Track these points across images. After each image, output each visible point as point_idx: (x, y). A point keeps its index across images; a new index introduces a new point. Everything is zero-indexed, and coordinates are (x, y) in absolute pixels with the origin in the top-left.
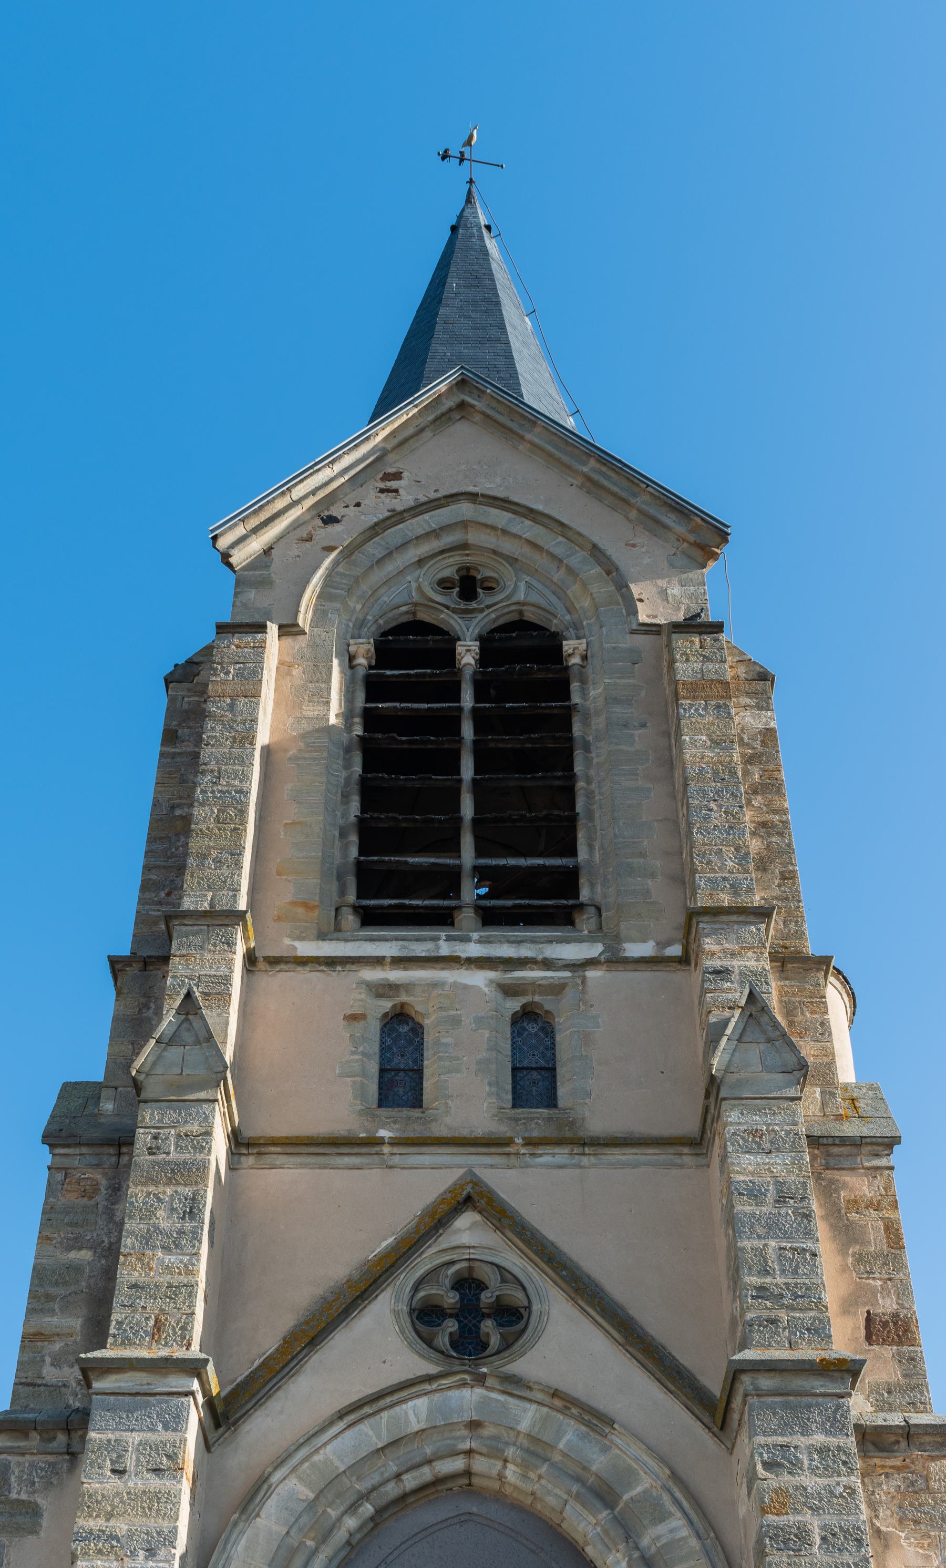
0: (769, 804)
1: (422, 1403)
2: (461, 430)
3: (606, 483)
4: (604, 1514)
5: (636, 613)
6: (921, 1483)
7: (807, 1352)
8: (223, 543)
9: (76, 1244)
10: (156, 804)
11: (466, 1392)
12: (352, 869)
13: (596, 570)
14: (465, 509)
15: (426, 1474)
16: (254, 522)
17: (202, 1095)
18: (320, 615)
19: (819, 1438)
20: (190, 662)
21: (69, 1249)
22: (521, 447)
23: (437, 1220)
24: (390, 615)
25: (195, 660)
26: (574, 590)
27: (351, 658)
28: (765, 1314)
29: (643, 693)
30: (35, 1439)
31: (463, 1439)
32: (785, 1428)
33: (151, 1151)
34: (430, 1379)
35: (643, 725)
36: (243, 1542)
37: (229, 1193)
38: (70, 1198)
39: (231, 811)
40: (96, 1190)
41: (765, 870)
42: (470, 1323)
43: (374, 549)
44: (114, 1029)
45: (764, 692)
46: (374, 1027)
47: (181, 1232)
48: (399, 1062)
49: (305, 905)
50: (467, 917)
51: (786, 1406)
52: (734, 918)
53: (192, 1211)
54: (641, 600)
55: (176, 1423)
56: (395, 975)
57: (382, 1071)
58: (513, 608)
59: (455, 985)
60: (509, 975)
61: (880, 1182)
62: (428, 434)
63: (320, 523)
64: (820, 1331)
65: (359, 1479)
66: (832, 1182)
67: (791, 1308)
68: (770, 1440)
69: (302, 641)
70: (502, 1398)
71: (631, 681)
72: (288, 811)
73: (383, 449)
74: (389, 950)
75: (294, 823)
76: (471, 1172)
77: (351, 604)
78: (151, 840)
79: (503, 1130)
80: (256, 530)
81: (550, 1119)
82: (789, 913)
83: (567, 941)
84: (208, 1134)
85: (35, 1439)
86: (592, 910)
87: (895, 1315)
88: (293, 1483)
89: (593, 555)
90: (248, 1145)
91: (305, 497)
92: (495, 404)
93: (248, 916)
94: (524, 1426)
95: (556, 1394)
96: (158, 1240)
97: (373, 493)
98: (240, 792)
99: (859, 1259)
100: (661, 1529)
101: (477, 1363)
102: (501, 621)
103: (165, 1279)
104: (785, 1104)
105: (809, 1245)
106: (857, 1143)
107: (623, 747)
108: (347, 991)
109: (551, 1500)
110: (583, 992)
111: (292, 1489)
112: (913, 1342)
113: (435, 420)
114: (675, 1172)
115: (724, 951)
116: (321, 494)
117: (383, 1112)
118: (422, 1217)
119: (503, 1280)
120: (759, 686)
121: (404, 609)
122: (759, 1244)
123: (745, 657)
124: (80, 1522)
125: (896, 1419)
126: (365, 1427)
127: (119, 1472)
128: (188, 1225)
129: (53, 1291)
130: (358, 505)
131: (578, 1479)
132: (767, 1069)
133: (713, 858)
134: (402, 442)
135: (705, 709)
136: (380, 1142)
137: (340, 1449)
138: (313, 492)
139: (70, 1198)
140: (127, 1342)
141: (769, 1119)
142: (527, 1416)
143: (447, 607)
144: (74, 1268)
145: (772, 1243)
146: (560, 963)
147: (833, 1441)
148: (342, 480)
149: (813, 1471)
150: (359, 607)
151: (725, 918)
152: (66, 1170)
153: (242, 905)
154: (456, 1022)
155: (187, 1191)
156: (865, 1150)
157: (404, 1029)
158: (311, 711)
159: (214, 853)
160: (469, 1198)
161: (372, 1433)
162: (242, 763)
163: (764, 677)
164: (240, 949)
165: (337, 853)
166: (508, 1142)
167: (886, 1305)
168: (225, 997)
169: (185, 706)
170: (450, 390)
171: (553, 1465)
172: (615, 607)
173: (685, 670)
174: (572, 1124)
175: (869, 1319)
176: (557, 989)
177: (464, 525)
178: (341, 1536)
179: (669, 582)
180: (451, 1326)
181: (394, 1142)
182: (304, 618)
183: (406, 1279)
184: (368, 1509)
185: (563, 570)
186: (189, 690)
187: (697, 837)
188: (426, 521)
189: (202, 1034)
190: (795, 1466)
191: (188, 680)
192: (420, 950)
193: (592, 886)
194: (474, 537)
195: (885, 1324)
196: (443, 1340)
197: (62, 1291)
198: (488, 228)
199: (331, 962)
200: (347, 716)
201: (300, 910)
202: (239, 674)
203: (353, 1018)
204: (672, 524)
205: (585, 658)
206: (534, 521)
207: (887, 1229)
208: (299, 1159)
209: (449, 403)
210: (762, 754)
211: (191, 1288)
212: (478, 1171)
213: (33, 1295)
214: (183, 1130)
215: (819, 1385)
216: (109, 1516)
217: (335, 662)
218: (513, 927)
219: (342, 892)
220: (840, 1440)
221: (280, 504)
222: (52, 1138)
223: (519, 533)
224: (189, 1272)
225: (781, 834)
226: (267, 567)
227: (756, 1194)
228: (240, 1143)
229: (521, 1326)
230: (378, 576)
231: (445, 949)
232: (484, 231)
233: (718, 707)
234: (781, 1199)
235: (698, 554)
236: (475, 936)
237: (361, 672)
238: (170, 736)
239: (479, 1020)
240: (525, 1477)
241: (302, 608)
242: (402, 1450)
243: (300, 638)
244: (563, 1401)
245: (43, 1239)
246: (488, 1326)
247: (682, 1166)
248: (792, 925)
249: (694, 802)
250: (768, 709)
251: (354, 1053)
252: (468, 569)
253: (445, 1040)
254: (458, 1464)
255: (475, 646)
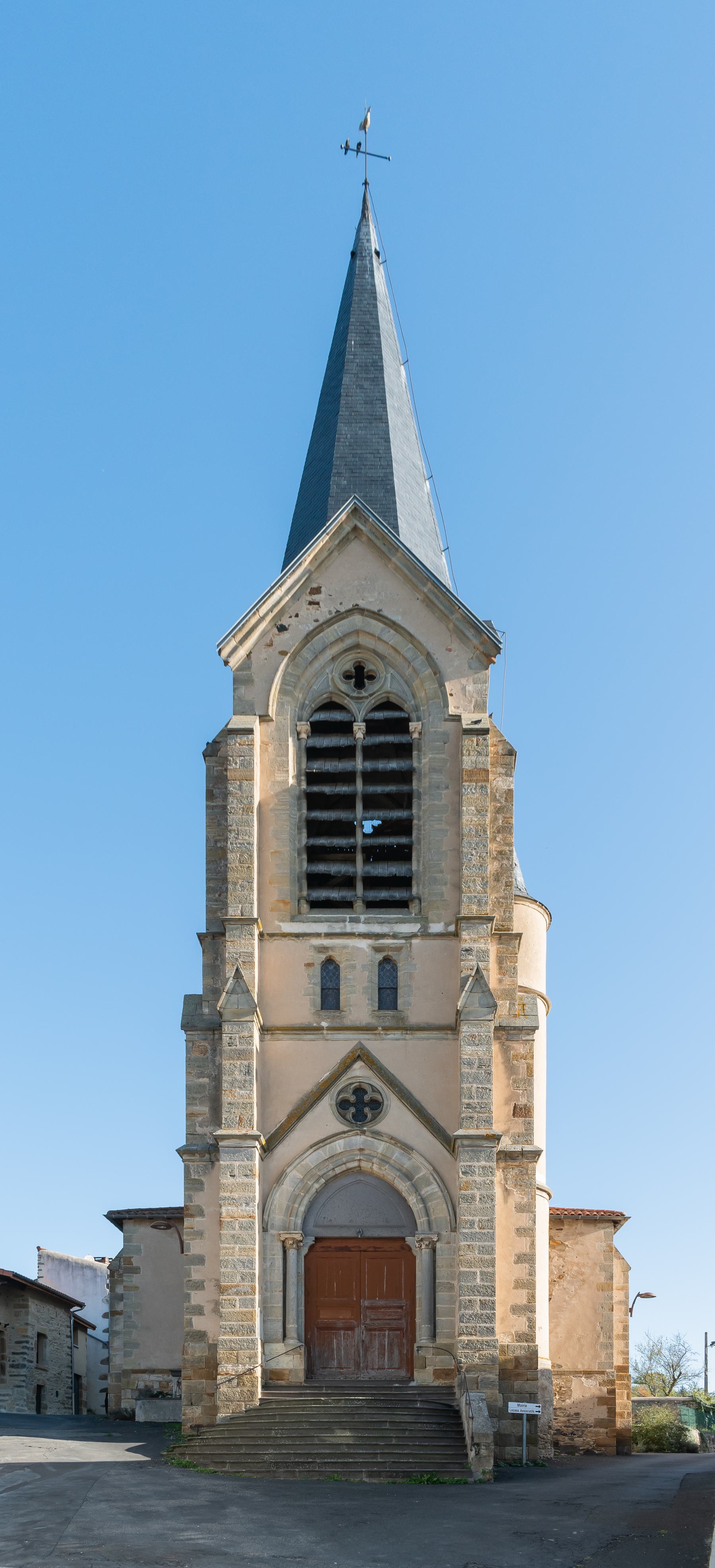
0: (504, 839)
1: (341, 1142)
2: (356, 548)
3: (437, 602)
4: (409, 1183)
5: (446, 705)
6: (525, 1172)
7: (483, 1132)
8: (225, 653)
9: (201, 1075)
10: (207, 840)
11: (358, 1137)
12: (304, 876)
13: (429, 671)
14: (357, 620)
15: (344, 1168)
16: (240, 636)
17: (247, 1018)
18: (281, 705)
19: (483, 1163)
20: (215, 742)
21: (199, 1077)
22: (390, 566)
23: (346, 1065)
24: (318, 700)
25: (217, 740)
26: (416, 683)
27: (298, 734)
28: (469, 1115)
29: (449, 764)
30: (197, 1157)
31: (357, 1155)
32: (471, 1159)
33: (230, 1045)
34: (344, 1132)
35: (447, 788)
36: (278, 1194)
37: (262, 1053)
38: (196, 1055)
39: (246, 856)
40: (206, 1051)
41: (498, 881)
42: (360, 1108)
43: (307, 654)
44: (204, 971)
45: (510, 764)
46: (318, 968)
47: (245, 1081)
48: (330, 985)
49: (284, 902)
50: (359, 905)
51: (472, 1151)
52: (477, 921)
53: (248, 1072)
54: (451, 695)
55: (251, 1158)
56: (327, 942)
57: (322, 989)
58: (384, 695)
59: (353, 947)
60: (378, 942)
61: (528, 1047)
62: (336, 554)
63: (275, 630)
64: (488, 1122)
65: (319, 1170)
66: (508, 1047)
67: (479, 1112)
68: (465, 1164)
69: (272, 725)
70: (371, 1139)
71: (443, 756)
72: (273, 845)
73: (310, 570)
74: (322, 928)
75: (275, 852)
76: (360, 1043)
77: (296, 694)
78: (208, 863)
79: (373, 1022)
80: (241, 642)
81: (394, 1017)
82: (507, 907)
83: (403, 921)
84: (252, 1037)
85: (197, 1157)
86: (417, 901)
87: (526, 1105)
88: (295, 1172)
89: (427, 659)
90: (267, 1031)
91: (266, 614)
92: (374, 530)
93: (259, 920)
94: (380, 1151)
95: (392, 1138)
96: (236, 1084)
97: (305, 606)
98: (249, 844)
99: (515, 1081)
100: (429, 1188)
101: (362, 1126)
102: (378, 703)
103: (241, 1101)
104: (486, 1023)
105: (488, 1086)
106: (521, 1029)
107: (436, 802)
108: (305, 953)
109: (390, 1177)
110: (410, 951)
111: (294, 1175)
112: (531, 1116)
113: (340, 542)
114: (444, 1042)
115: (471, 939)
116: (276, 610)
117: (323, 1013)
118: (340, 1064)
119: (373, 1091)
120: (508, 759)
121: (325, 696)
122: (469, 1085)
123: (503, 739)
124: (221, 1194)
125: (518, 1148)
126: (320, 1151)
127: (233, 1176)
128: (248, 1078)
129: (195, 1095)
130: (297, 616)
131: (399, 1170)
132: (481, 1006)
133: (471, 885)
134: (320, 563)
135: (475, 789)
136: (322, 1028)
137: (312, 1159)
138: (271, 610)
139: (196, 1055)
140: (229, 1127)
141: (479, 1030)
142: (381, 1147)
143: (348, 695)
144: (201, 1086)
145: (475, 1085)
146: (401, 935)
147: (488, 1164)
148: (287, 599)
149: (479, 1175)
150: (301, 696)
151: (473, 921)
152: (193, 1042)
153: (255, 916)
154: (353, 967)
155: (246, 1063)
156: (524, 1032)
157: (331, 967)
158: (279, 777)
159: (240, 882)
160: (361, 1055)
161: (323, 1153)
162: (249, 826)
163: (511, 753)
164: (256, 932)
165: (297, 868)
166: (375, 1029)
167: (522, 1101)
168: (252, 963)
169: (215, 773)
170: (348, 517)
171: (391, 1165)
172: (437, 700)
173: (468, 761)
174: (403, 1019)
175: (515, 1107)
176: (399, 949)
177: (357, 632)
178: (313, 1190)
179: (467, 681)
180: (353, 1110)
181: (329, 1029)
182: (272, 711)
183: (335, 1090)
184: (323, 1181)
185: (411, 668)
186: (216, 762)
187: (465, 872)
188: (336, 630)
189: (245, 989)
190: (474, 1172)
191: (215, 751)
192: (337, 928)
193: (418, 885)
194: (363, 640)
195: (521, 1109)
196: (349, 1116)
197: (199, 1096)
198: (378, 253)
199: (297, 936)
200: (298, 777)
201: (281, 905)
202: (242, 765)
203: (309, 965)
204: (471, 637)
205: (420, 733)
206: (396, 630)
207: (528, 1068)
208: (289, 1036)
209: (348, 528)
210: (505, 807)
211: (251, 1104)
212: (363, 1042)
213: (188, 1098)
214: (241, 1035)
215: (486, 1144)
216: (231, 1192)
217: (290, 739)
218: (382, 910)
219: (301, 890)
220: (491, 1164)
221: (253, 621)
222: (185, 1027)
223: (387, 640)
224: (250, 1098)
225: (508, 859)
226: (249, 668)
227: (470, 1064)
228: (264, 1030)
229: (379, 1110)
230: (311, 670)
231: (349, 927)
232: (374, 255)
233: (482, 787)
234: (480, 1067)
235: (484, 659)
236: (362, 917)
237: (304, 743)
238: (210, 795)
239: (364, 966)
240: (380, 1169)
241: (271, 704)
242: (335, 1159)
243: (271, 723)
244: (395, 1141)
245: (188, 1073)
246: (367, 1110)
247: (447, 1039)
248: (507, 914)
249: (465, 850)
250: (511, 776)
251: (309, 983)
252: (360, 662)
253: (349, 977)
254: (356, 1164)
255: (363, 725)
